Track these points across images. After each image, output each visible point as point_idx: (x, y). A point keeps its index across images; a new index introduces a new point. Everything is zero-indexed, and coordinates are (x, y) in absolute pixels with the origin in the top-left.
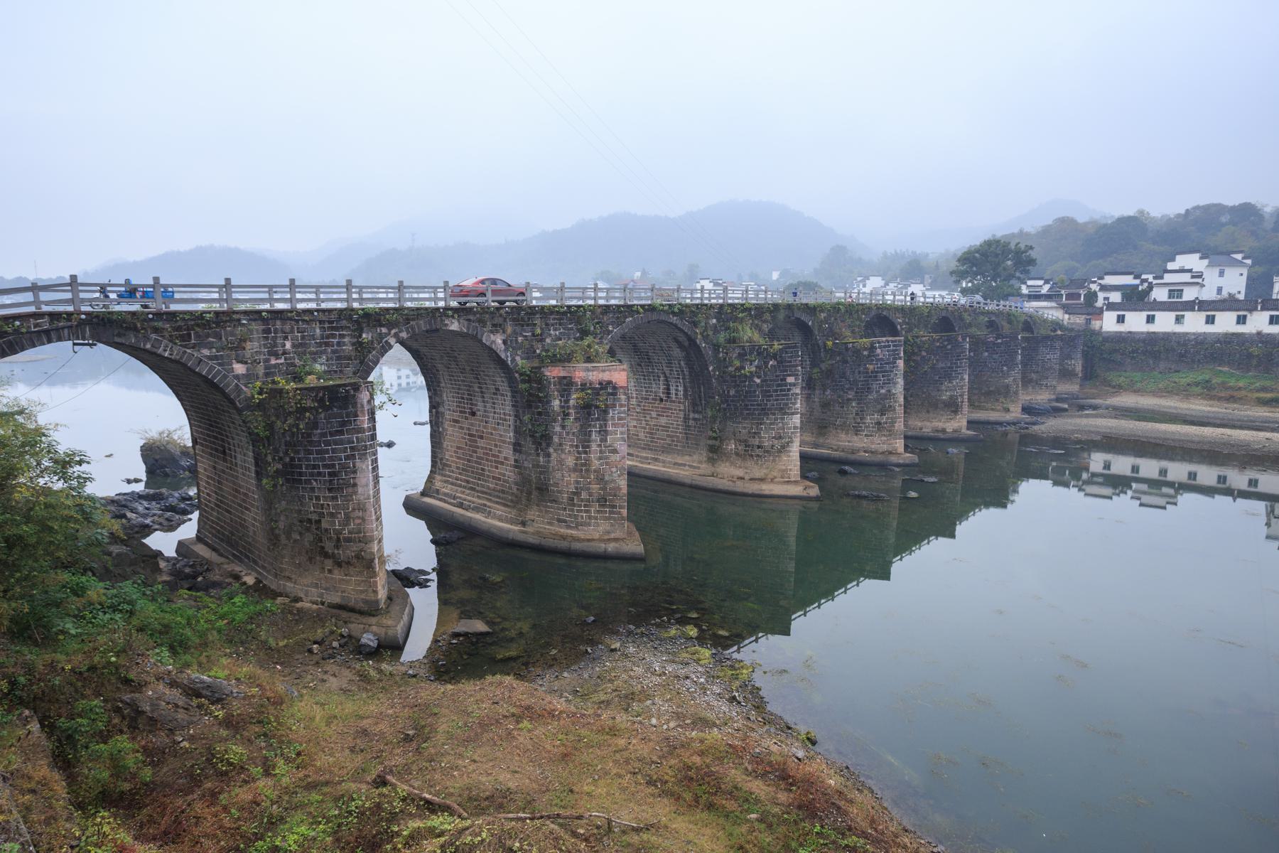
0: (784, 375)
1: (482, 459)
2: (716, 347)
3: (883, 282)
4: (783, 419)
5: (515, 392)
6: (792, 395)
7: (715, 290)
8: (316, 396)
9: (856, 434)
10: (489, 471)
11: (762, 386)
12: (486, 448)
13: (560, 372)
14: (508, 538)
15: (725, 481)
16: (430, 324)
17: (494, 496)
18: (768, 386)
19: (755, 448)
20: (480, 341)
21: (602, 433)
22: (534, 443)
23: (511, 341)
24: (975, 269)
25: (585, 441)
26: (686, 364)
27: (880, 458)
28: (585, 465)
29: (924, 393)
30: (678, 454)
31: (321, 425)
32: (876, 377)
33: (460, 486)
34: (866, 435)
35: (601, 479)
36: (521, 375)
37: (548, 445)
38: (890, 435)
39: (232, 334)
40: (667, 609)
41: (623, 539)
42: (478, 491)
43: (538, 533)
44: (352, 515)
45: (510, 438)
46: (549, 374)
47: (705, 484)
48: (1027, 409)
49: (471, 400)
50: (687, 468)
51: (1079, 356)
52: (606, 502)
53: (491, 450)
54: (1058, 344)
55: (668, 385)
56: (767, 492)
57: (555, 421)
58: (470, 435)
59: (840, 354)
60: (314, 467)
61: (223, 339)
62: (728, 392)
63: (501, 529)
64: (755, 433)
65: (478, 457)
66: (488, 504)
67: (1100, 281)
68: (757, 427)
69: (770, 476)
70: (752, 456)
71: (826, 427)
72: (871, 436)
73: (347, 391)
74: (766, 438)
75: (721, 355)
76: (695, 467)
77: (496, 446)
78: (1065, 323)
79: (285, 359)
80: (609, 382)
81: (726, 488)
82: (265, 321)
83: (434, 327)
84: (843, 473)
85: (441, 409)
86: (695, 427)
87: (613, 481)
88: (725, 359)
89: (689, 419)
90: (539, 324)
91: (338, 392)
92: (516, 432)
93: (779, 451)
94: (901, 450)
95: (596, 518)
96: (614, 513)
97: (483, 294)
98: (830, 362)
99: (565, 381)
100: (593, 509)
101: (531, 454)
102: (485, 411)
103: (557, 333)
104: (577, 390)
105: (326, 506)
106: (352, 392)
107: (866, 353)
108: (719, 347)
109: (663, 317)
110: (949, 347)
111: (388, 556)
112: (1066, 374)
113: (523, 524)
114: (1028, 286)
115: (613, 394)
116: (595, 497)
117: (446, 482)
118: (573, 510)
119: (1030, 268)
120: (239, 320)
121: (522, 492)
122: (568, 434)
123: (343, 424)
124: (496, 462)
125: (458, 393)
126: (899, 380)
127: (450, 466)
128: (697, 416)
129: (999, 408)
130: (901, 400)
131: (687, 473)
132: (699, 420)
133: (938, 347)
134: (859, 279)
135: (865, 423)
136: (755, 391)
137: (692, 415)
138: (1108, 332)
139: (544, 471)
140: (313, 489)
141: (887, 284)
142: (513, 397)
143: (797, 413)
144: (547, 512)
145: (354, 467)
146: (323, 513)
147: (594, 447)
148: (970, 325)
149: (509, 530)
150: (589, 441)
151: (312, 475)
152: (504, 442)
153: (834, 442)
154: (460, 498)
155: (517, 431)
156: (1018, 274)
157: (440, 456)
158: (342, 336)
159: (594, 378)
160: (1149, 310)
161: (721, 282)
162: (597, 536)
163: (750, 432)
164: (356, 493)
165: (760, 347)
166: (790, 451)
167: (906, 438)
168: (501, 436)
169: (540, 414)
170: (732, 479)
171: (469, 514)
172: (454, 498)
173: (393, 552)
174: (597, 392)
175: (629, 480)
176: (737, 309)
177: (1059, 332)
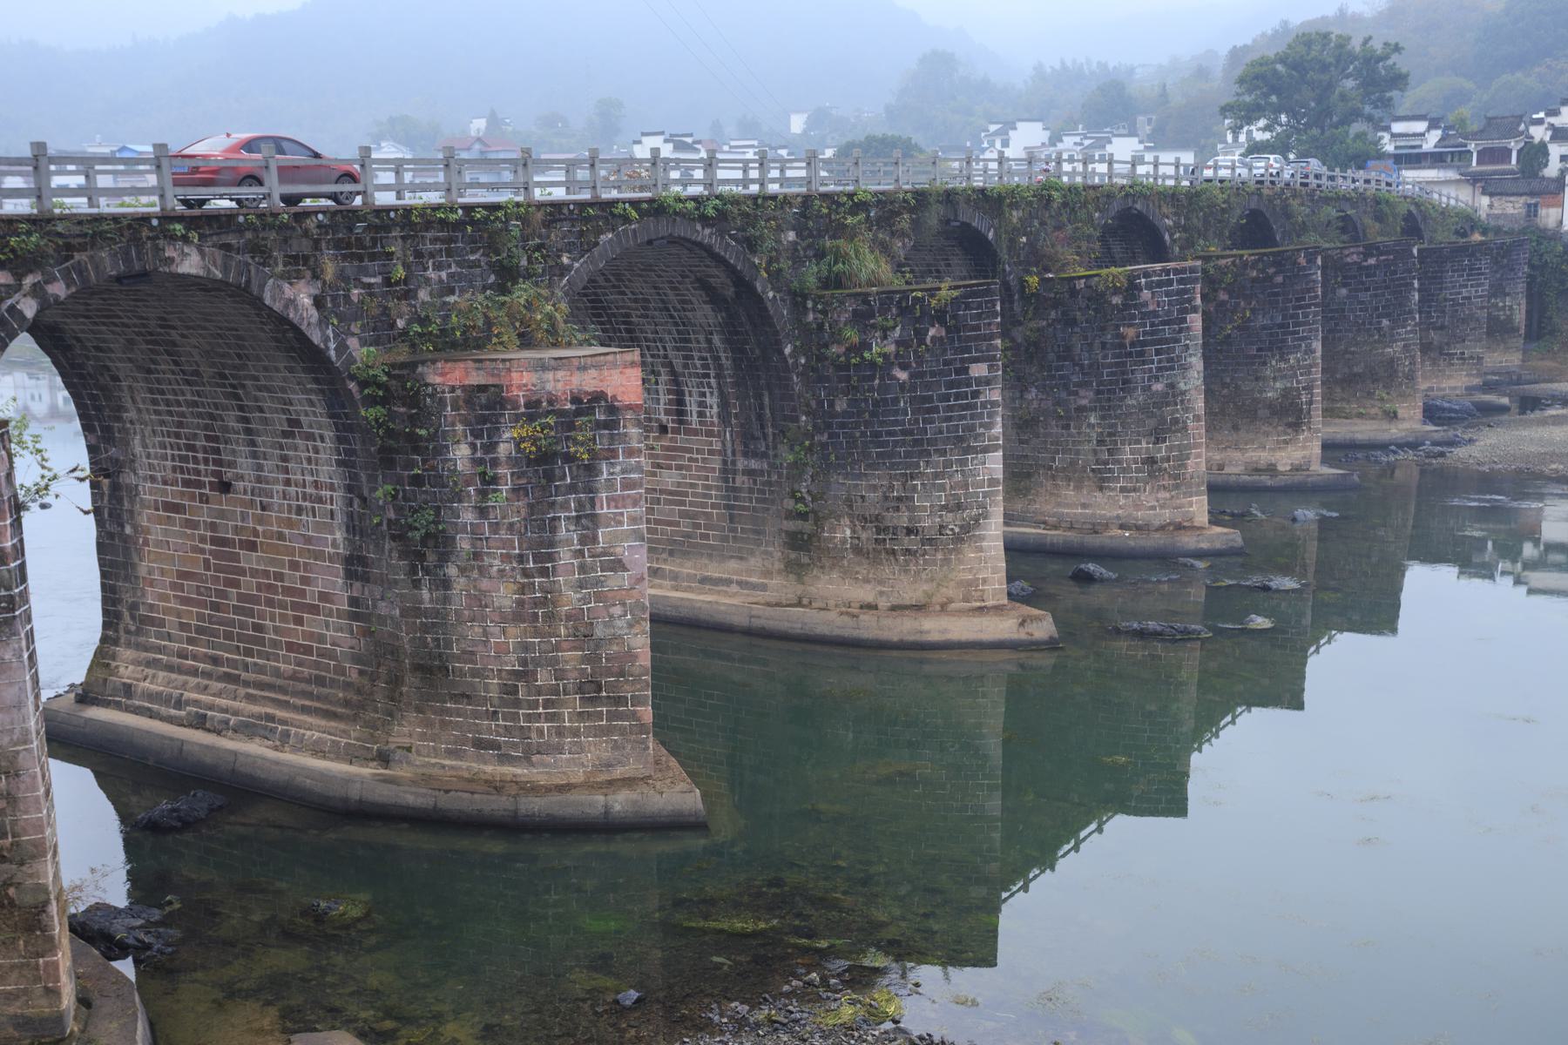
0: (963, 360)
1: (254, 600)
2: (798, 299)
3: (1048, 133)
4: (963, 463)
5: (345, 429)
6: (984, 405)
7: (678, 161)
9: (1101, 489)
10: (276, 630)
11: (913, 388)
12: (266, 574)
13: (467, 373)
14: (346, 800)
15: (832, 615)
16: (127, 260)
17: (295, 694)
18: (928, 386)
20: (257, 302)
21: (584, 521)
22: (403, 555)
23: (334, 299)
24: (1274, 98)
25: (541, 544)
26: (727, 341)
27: (1157, 540)
28: (543, 602)
29: (1225, 385)
30: (710, 556)
32: (1141, 354)
33: (194, 672)
34: (1123, 490)
35: (584, 636)
36: (364, 384)
37: (444, 558)
38: (1177, 487)
40: (806, 950)
41: (645, 779)
42: (247, 684)
43: (426, 780)
45: (334, 544)
46: (438, 380)
47: (784, 626)
48: (1432, 413)
49: (217, 451)
50: (734, 588)
51: (1521, 287)
52: (600, 690)
53: (279, 577)
54: (1484, 263)
55: (680, 393)
56: (935, 637)
57: (459, 497)
58: (214, 541)
59: (1056, 304)
62: (831, 404)
63: (323, 776)
64: (899, 499)
65: (241, 597)
66: (280, 713)
67: (1552, 120)
68: (904, 485)
69: (938, 599)
70: (893, 552)
71: (1029, 475)
72: (1135, 490)
74: (927, 510)
75: (811, 317)
76: (754, 587)
77: (294, 566)
78: (1483, 215)
80: (598, 397)
81: (837, 632)
83: (137, 267)
84: (1085, 579)
85: (128, 478)
86: (751, 491)
87: (616, 638)
88: (821, 327)
89: (735, 472)
90: (399, 254)
92: (351, 528)
93: (957, 540)
94: (1202, 518)
95: (575, 733)
96: (620, 717)
97: (254, 179)
98: (1033, 325)
99: (483, 398)
101: (396, 582)
102: (259, 480)
103: (444, 275)
104: (517, 418)
107: (1117, 300)
108: (805, 297)
109: (681, 230)
110: (1279, 279)
111: (73, 889)
112: (1498, 330)
113: (384, 759)
114: (1394, 136)
116: (572, 679)
117: (149, 664)
118: (515, 717)
119: (1395, 94)
121: (373, 678)
122: (495, 527)
124: (295, 606)
125: (178, 436)
126: (1194, 360)
127: (162, 623)
128: (754, 464)
129: (1373, 411)
130: (1199, 405)
131: (735, 601)
132: (762, 472)
133: (1254, 280)
134: (993, 128)
135: (1119, 462)
136: (896, 401)
137: (741, 463)
139: (437, 621)
141: (1055, 139)
142: (339, 440)
143: (995, 448)
144: (444, 724)
147: (565, 557)
148: (1304, 228)
149: (348, 780)
150: (552, 544)
152: (319, 555)
153: (1048, 508)
154: (196, 703)
155: (353, 527)
156: (1368, 109)
157: (128, 598)
159: (560, 386)
161: (689, 140)
162: (578, 776)
163: (886, 498)
165: (905, 294)
166: (982, 538)
167: (1214, 490)
168: (308, 540)
169: (417, 481)
170: (846, 608)
171: (227, 743)
172: (179, 704)
173: (88, 875)
174: (567, 423)
175: (654, 635)
176: (839, 204)
177: (1477, 237)
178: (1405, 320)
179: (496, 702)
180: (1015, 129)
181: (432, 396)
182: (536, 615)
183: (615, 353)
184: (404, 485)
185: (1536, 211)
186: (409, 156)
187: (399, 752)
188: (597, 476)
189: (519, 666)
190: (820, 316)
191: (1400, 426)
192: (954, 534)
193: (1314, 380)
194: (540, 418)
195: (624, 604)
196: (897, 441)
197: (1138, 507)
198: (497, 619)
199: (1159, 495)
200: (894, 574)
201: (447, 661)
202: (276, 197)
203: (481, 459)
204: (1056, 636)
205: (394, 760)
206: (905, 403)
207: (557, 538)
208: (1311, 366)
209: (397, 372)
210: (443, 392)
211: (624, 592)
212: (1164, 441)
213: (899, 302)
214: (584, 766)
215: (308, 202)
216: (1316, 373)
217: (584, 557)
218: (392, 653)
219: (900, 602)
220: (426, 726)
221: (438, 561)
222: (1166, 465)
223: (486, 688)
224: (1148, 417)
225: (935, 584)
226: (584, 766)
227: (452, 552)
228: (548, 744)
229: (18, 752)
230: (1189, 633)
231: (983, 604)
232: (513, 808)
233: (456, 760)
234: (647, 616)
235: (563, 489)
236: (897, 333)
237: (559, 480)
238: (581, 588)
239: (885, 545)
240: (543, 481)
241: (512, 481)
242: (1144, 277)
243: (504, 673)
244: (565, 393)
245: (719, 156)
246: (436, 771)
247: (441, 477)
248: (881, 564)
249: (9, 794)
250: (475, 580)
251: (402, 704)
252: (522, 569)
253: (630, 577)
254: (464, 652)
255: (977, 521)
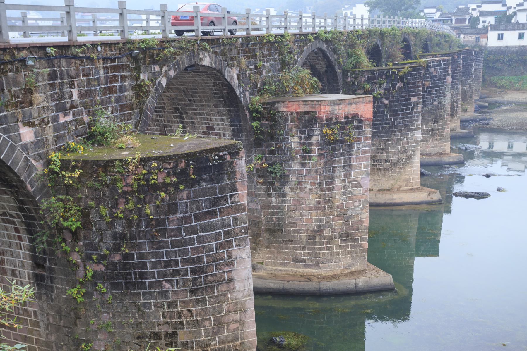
0: (409, 96)
4: (407, 135)
6: (415, 113)
8: (176, 167)
11: (390, 107)
13: (299, 107)
19: (383, 163)
21: (346, 168)
25: (329, 178)
28: (328, 202)
31: (181, 207)
32: (430, 91)
35: (344, 215)
36: (251, 112)
37: (283, 184)
38: (441, 139)
39: (16, 83)
43: (274, 276)
44: (226, 320)
46: (285, 110)
52: (348, 236)
56: (398, 201)
60: (168, 264)
61: (6, 91)
64: (383, 149)
68: (385, 144)
69: (396, 186)
70: (380, 169)
72: (426, 141)
73: (221, 158)
75: (349, 79)
79: (74, 115)
80: (355, 116)
82: (47, 57)
87: (356, 215)
88: (354, 83)
91: (208, 160)
93: (404, 164)
94: (448, 151)
95: (338, 254)
96: (355, 246)
100: (334, 246)
101: (259, 195)
105: (185, 313)
106: (228, 158)
108: (348, 71)
115: (358, 128)
116: (338, 232)
120: (23, 61)
123: (216, 201)
126: (448, 93)
136: (383, 111)
138: (491, 47)
139: (279, 210)
140: (165, 294)
144: (279, 253)
145: (230, 257)
146: (181, 323)
147: (338, 183)
150: (333, 178)
151: (164, 275)
158: (123, 78)
160: (521, 29)
162: (338, 271)
163: (378, 149)
164: (231, 291)
169: (272, 152)
175: (370, 215)
178: (470, 77)
179: (305, 243)
180: (355, 6)
181: (281, 117)
182: (325, 207)
183: (363, 97)
184: (266, 154)
185: (479, 40)
186: (41, 17)
187: (259, 265)
188: (353, 149)
189: (317, 228)
190: (353, 79)
191: (468, 114)
192: (403, 162)
193: (459, 99)
194: (331, 125)
195: (360, 201)
196: (383, 127)
197: (427, 147)
198: (307, 209)
199: (435, 143)
200: (380, 177)
201: (282, 227)
202: (200, 31)
203: (304, 143)
204: (441, 198)
205: (258, 269)
206: (387, 113)
207: (335, 175)
208: (458, 94)
209: (265, 106)
210: (287, 115)
211: (360, 196)
212: (437, 123)
213: (386, 73)
214: (340, 267)
215: (215, 33)
216: (459, 96)
217: (345, 182)
218: (256, 224)
219: (382, 188)
220: (271, 254)
221: (280, 186)
222: (437, 131)
223: (300, 237)
224: (432, 114)
225: (395, 181)
226: (340, 267)
227: (287, 182)
228: (327, 260)
229: (246, 301)
230: (484, 195)
231: (412, 188)
232: (318, 287)
233: (284, 267)
234: (368, 205)
235: (339, 154)
236: (385, 85)
237: (338, 151)
238: (344, 195)
239: (377, 166)
240: (332, 152)
241: (318, 152)
242: (432, 63)
243: (309, 231)
244: (342, 114)
245: (304, 15)
246: (277, 272)
247: (284, 151)
248: (375, 174)
249: (240, 320)
250: (298, 193)
251: (259, 245)
252: (321, 188)
253: (363, 190)
254: (291, 223)
255: (411, 156)
